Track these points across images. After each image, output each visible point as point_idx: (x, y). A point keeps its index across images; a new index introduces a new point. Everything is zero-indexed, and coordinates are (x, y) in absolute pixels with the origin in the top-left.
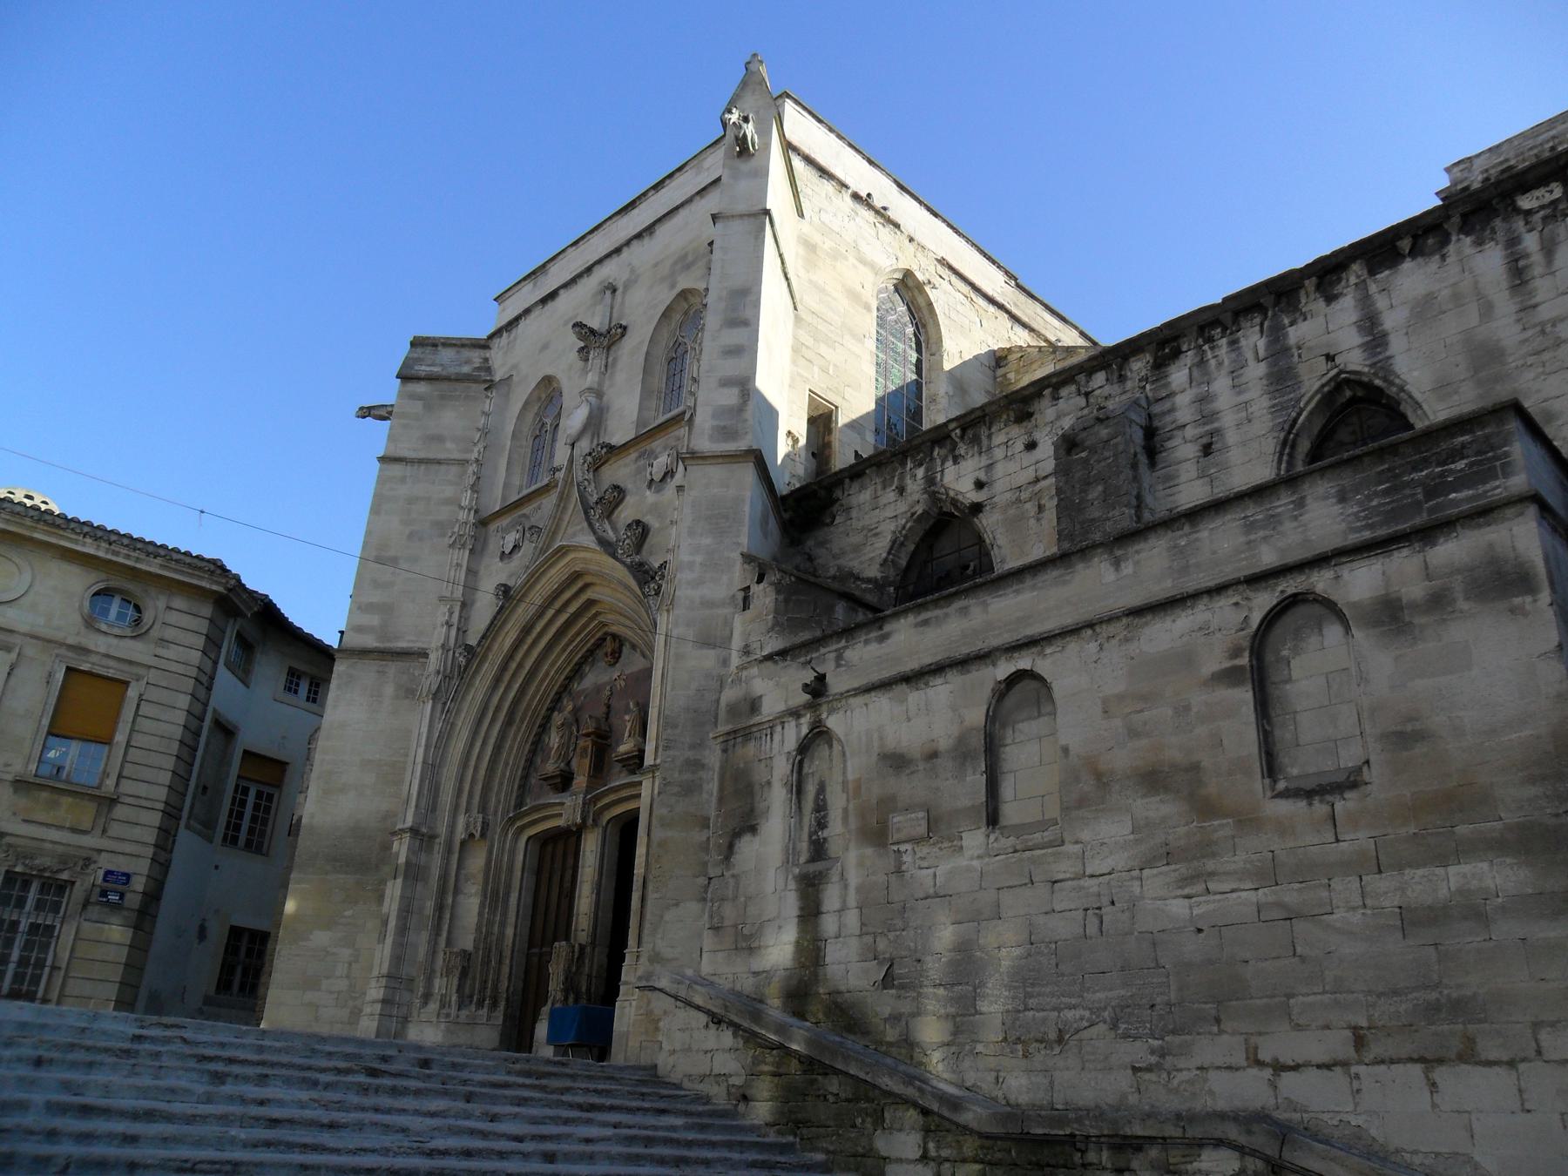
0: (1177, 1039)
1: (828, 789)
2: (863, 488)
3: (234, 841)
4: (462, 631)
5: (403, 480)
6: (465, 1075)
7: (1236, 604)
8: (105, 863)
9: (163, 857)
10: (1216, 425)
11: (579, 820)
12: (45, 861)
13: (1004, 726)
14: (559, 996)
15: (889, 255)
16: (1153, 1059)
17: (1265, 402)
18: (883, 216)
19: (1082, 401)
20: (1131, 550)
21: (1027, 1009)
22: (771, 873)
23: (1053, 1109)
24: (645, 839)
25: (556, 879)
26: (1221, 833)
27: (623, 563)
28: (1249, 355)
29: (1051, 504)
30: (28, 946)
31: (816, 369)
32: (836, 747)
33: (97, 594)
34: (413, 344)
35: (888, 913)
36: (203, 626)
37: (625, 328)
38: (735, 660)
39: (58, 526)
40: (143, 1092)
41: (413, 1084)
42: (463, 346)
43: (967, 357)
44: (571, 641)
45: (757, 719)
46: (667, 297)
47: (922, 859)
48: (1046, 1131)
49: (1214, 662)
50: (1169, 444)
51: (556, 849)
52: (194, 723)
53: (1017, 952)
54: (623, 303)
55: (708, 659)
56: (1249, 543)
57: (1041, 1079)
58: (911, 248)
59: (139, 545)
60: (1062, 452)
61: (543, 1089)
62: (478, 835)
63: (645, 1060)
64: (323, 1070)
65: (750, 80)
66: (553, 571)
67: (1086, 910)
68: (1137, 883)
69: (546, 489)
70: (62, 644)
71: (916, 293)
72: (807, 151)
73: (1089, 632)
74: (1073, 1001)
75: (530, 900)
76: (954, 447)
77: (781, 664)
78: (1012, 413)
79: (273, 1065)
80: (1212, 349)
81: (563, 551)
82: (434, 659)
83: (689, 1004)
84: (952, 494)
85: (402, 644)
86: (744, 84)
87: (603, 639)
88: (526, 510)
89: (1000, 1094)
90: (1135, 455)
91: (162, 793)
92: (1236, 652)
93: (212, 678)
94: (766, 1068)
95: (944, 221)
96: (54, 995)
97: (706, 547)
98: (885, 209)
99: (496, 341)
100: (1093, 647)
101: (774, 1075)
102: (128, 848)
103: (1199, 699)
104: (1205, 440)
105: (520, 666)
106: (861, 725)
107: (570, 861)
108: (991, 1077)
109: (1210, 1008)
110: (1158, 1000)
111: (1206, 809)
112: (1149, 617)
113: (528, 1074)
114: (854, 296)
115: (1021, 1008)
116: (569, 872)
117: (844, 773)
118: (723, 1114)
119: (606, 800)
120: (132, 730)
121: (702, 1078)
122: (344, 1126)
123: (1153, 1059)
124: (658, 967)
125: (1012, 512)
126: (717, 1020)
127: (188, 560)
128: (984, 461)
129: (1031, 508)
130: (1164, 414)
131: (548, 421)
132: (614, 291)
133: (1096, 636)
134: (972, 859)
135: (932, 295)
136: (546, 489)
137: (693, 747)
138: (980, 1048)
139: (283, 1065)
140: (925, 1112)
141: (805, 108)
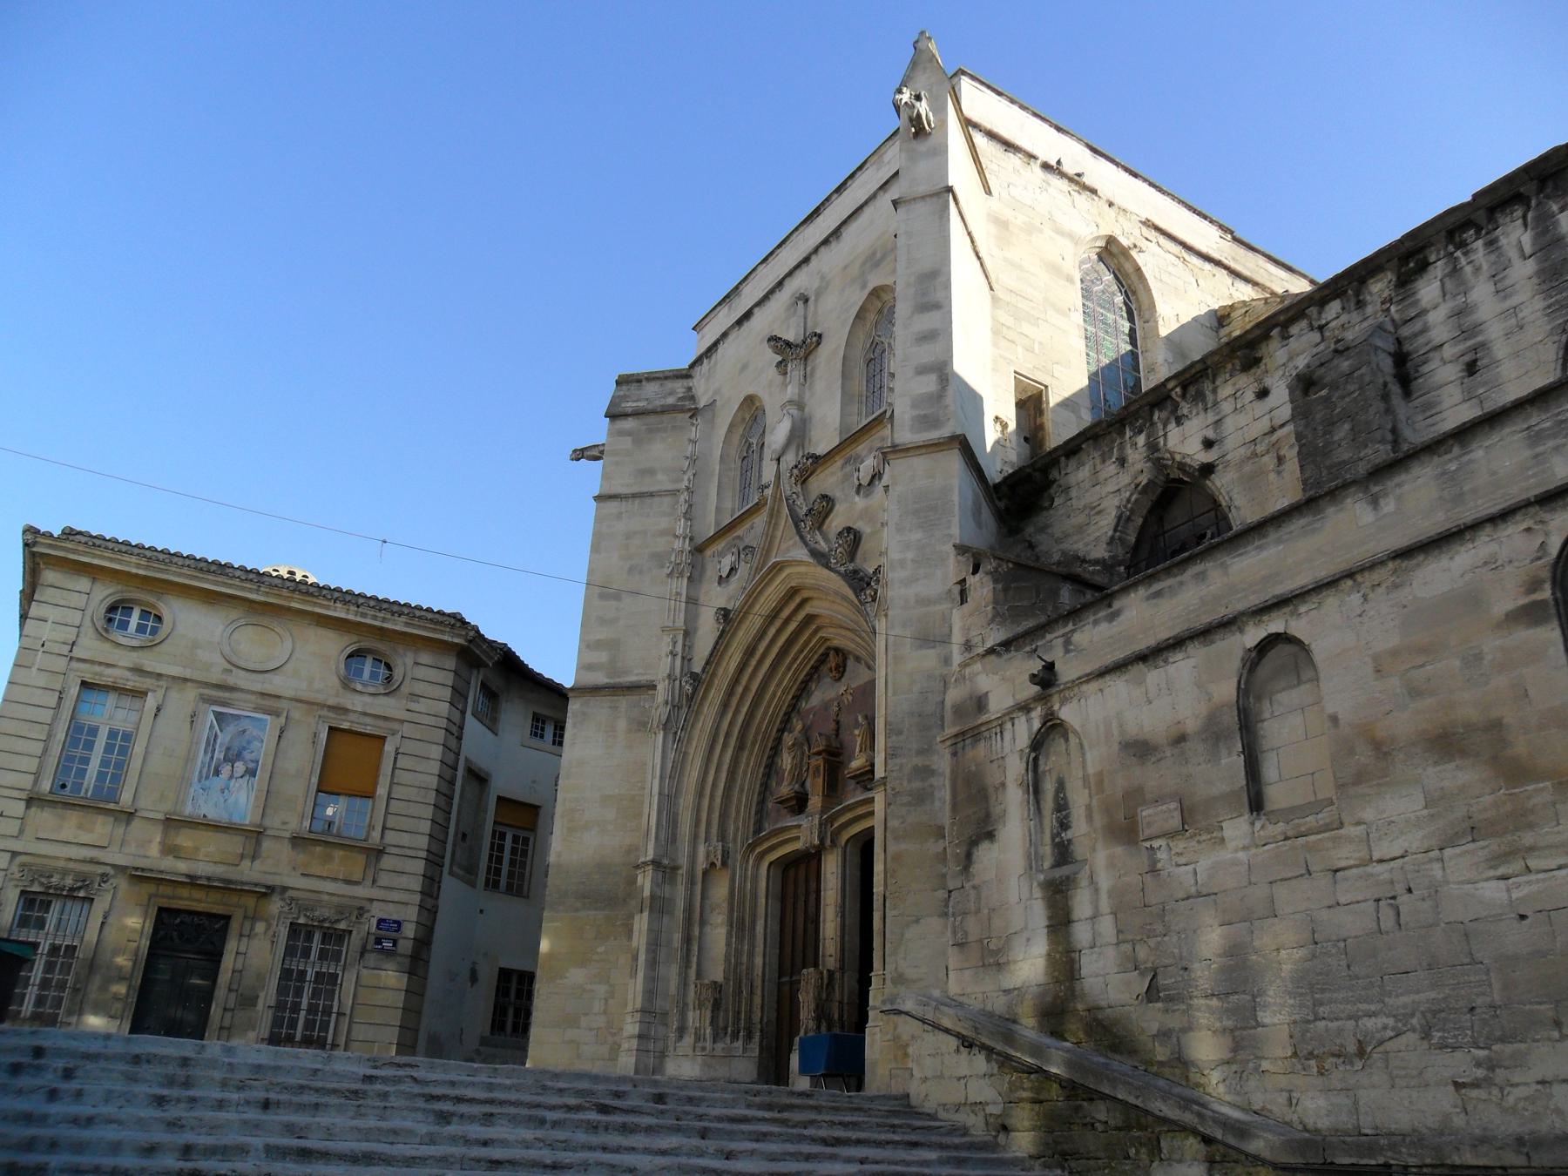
0: (1509, 1049)
1: (1068, 786)
2: (1081, 464)
3: (496, 885)
4: (687, 660)
5: (619, 516)
6: (701, 1110)
7: (1528, 530)
8: (378, 911)
9: (429, 903)
10: (1480, 339)
11: (817, 842)
12: (326, 913)
13: (1259, 699)
14: (812, 1025)
15: (1086, 224)
16: (1480, 1073)
17: (1539, 304)
18: (1077, 183)
19: (1316, 336)
20: (1390, 484)
21: (1317, 1019)
22: (1014, 882)
23: (1360, 1134)
24: (882, 857)
25: (801, 904)
26: (1537, 800)
27: (838, 572)
28: (1513, 254)
29: (1291, 454)
30: (316, 994)
31: (1020, 349)
32: (1073, 740)
33: (350, 656)
34: (618, 383)
35: (1146, 917)
36: (449, 678)
37: (820, 336)
38: (957, 658)
39: (312, 595)
40: (366, 1134)
41: (646, 1120)
42: (666, 378)
43: (1185, 319)
44: (795, 659)
45: (984, 718)
46: (858, 297)
47: (1178, 854)
48: (1353, 1160)
49: (1507, 599)
50: (1425, 369)
51: (798, 873)
52: (448, 773)
53: (1299, 954)
54: (816, 312)
55: (928, 659)
56: (1537, 456)
57: (1343, 1100)
58: (1112, 212)
59: (385, 606)
60: (1298, 393)
61: (784, 1122)
62: (719, 864)
63: (896, 1089)
64: (553, 1108)
65: (920, 59)
66: (770, 590)
67: (1378, 900)
68: (1437, 866)
69: (757, 508)
70: (323, 706)
71: (1122, 260)
72: (989, 126)
73: (1349, 582)
74: (1373, 1008)
75: (777, 928)
76: (1176, 406)
77: (1006, 656)
78: (1237, 362)
79: (502, 1103)
80: (1465, 254)
81: (778, 567)
82: (662, 689)
83: (937, 1027)
84: (1178, 458)
85: (632, 678)
86: (914, 64)
87: (826, 655)
88: (739, 532)
89: (1295, 1118)
90: (1385, 385)
91: (423, 842)
92: (1534, 585)
93: (461, 728)
94: (1025, 1095)
95: (1145, 180)
96: (342, 1040)
97: (918, 541)
98: (1079, 175)
99: (698, 369)
100: (1355, 598)
101: (1035, 1101)
102: (396, 896)
103: (1492, 645)
104: (1467, 358)
105: (747, 688)
106: (1098, 713)
107: (813, 885)
108: (1282, 1099)
109: (1546, 1010)
110: (1479, 1001)
111: (1515, 773)
112: (1421, 558)
113: (769, 1107)
114: (1054, 269)
115: (1311, 1018)
116: (813, 897)
117: (1084, 767)
118: (983, 1146)
119: (843, 820)
120: (392, 783)
121: (958, 1108)
122: (569, 1167)
123: (1480, 1073)
124: (902, 990)
125: (1247, 468)
126: (967, 1043)
127: (430, 616)
128: (1211, 417)
129: (1269, 461)
130: (1415, 335)
131: (754, 441)
132: (806, 301)
133: (1358, 585)
134: (1236, 851)
135: (1140, 259)
136: (757, 508)
137: (921, 752)
138: (1265, 1065)
139: (512, 1103)
140: (1207, 1140)
141: (982, 83)
